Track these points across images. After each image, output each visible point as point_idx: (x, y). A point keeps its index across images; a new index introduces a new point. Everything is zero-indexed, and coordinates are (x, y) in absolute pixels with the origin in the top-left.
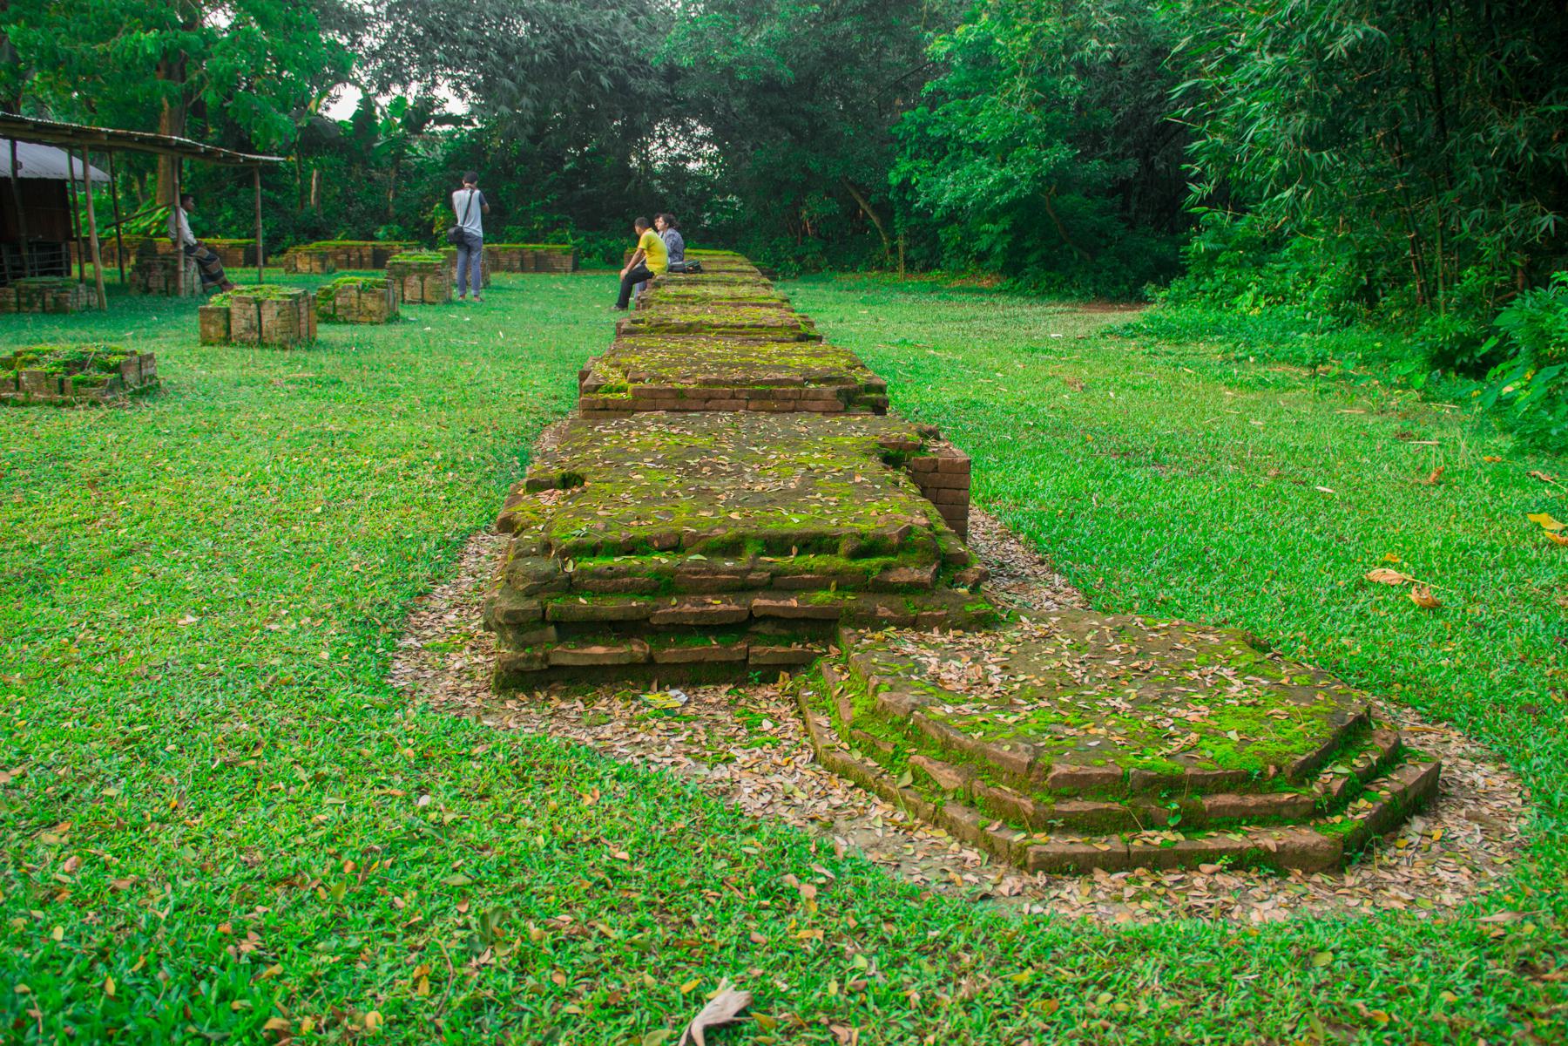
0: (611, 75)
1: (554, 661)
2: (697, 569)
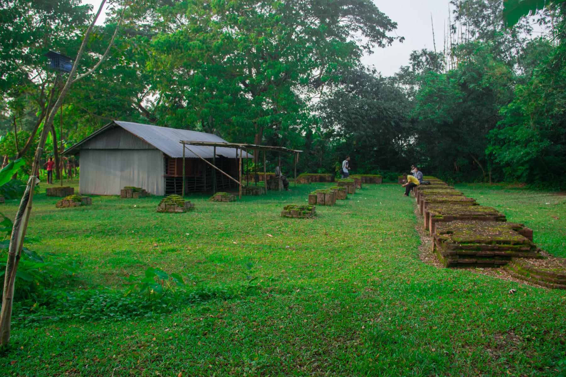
0: (394, 122)
1: (459, 262)
2: (484, 246)
